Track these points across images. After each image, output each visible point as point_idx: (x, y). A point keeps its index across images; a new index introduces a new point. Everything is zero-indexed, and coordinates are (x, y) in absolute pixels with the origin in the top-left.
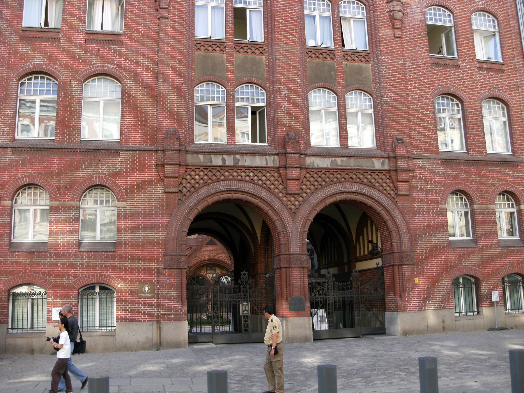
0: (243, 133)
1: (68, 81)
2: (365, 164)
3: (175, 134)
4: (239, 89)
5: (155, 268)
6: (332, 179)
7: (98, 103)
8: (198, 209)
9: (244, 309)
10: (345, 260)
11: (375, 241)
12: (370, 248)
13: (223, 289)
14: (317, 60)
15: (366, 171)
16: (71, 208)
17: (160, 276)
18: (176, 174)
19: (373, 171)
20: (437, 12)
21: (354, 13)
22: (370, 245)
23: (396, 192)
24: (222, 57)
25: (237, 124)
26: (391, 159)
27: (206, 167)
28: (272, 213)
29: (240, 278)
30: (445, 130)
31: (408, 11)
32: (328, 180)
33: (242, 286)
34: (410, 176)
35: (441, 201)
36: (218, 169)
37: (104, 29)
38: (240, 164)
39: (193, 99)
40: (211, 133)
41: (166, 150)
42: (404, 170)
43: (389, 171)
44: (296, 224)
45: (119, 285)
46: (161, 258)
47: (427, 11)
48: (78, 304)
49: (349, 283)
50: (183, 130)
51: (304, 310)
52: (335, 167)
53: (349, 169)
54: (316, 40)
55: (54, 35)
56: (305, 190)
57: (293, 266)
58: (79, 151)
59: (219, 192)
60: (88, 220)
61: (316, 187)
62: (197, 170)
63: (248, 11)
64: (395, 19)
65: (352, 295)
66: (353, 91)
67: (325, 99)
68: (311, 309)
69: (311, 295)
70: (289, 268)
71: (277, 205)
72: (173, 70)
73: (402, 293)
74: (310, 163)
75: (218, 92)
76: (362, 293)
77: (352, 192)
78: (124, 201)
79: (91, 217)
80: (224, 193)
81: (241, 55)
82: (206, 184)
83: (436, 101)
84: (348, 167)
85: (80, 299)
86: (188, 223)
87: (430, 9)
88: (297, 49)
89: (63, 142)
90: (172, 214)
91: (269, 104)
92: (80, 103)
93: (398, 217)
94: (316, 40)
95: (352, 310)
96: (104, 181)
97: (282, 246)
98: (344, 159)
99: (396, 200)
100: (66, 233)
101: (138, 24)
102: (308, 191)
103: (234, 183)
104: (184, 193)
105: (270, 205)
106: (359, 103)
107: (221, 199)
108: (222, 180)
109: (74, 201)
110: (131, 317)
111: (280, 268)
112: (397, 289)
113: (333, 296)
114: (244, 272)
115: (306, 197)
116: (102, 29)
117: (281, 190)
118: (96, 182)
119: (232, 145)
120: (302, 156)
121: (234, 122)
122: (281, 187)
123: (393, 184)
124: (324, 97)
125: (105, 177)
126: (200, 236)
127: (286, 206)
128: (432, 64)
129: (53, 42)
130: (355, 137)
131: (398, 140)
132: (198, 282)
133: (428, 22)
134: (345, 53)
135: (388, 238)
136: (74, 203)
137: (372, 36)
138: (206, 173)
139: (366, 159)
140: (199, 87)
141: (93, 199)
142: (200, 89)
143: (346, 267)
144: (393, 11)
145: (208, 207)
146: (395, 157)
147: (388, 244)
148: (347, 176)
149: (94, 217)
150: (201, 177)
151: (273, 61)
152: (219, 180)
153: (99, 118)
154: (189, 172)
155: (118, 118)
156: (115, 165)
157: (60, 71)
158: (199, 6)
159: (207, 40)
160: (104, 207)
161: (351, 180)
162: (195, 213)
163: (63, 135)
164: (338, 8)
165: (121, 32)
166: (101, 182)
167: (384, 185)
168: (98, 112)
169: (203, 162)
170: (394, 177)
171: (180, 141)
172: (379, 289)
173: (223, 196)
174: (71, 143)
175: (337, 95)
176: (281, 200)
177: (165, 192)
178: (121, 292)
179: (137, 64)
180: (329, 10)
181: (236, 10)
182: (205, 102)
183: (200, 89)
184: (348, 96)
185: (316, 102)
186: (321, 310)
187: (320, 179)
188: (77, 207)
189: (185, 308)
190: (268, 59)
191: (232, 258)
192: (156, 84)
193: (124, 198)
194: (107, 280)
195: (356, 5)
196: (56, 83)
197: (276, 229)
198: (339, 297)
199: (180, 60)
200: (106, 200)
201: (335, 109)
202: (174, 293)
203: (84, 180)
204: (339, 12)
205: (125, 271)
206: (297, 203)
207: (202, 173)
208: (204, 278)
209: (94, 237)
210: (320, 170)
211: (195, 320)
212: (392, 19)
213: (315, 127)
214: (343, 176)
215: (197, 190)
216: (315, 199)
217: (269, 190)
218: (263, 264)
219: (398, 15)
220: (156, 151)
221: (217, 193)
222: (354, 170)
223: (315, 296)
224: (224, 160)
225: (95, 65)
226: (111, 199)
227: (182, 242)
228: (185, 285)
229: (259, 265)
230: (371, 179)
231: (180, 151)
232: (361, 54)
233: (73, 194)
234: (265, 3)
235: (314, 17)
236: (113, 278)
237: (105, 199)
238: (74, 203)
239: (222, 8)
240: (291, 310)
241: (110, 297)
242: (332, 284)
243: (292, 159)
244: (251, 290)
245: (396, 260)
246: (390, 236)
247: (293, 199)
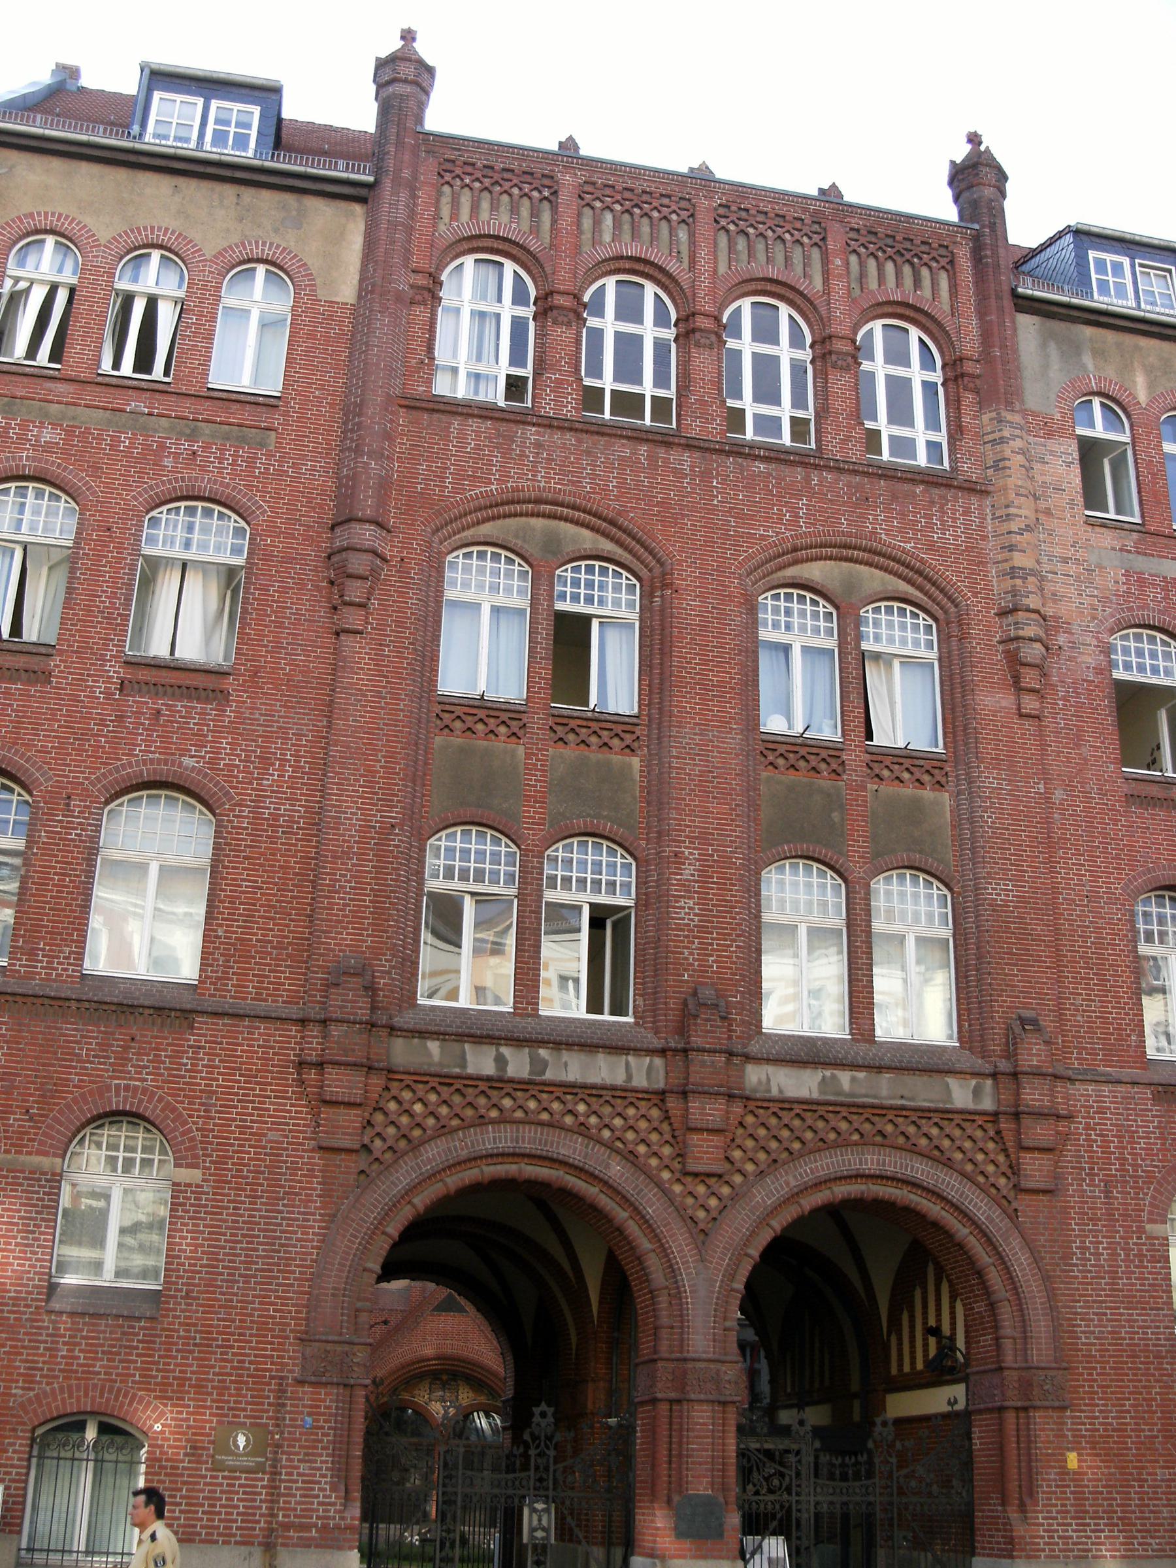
0: (564, 979)
1: (62, 798)
2: (923, 1092)
3: (361, 974)
4: (558, 851)
5: (272, 1377)
6: (821, 1135)
7: (143, 868)
8: (414, 1206)
9: (535, 1523)
10: (855, 1387)
11: (946, 1330)
12: (932, 1352)
13: (477, 1454)
14: (791, 777)
15: (925, 1113)
16: (35, 1175)
17: (284, 1405)
18: (357, 1095)
19: (947, 1114)
20: (1146, 646)
21: (904, 641)
22: (932, 1341)
23: (1014, 1179)
24: (513, 754)
25: (544, 952)
26: (1001, 1078)
27: (447, 1080)
28: (636, 1228)
29: (528, 1424)
30: (1164, 992)
31: (1062, 639)
32: (809, 1135)
33: (532, 1452)
34: (1058, 1133)
35: (1151, 1213)
36: (483, 1086)
37: (177, 655)
38: (549, 1075)
39: (420, 873)
40: (469, 977)
41: (331, 1020)
42: (1040, 1115)
43: (995, 1116)
44: (707, 1268)
45: (158, 1422)
46: (291, 1348)
47: (1116, 640)
48: (27, 1474)
49: (863, 1458)
50: (384, 963)
51: (721, 1535)
52: (831, 1098)
53: (873, 1107)
54: (789, 717)
55: (34, 663)
56: (738, 1165)
57: (693, 1396)
58: (74, 1005)
59: (481, 1157)
60: (83, 1212)
61: (774, 1156)
62: (421, 1086)
63: (595, 624)
64: (1023, 664)
65: (871, 1498)
66: (894, 873)
67: (810, 893)
68: (744, 1534)
69: (744, 1490)
70: (679, 1401)
71: (653, 1207)
72: (369, 784)
73: (1028, 1501)
74: (760, 1082)
75: (495, 855)
76: (901, 1492)
77: (882, 1177)
78: (195, 1166)
79: (94, 1203)
80: (495, 1160)
81: (570, 753)
82: (443, 1130)
83: (1140, 909)
84: (870, 1100)
85: (34, 1461)
86: (382, 1247)
87: (1125, 638)
88: (734, 739)
89: (29, 976)
90: (334, 1216)
91: (643, 901)
92: (91, 863)
93: (1020, 1261)
94: (789, 717)
95: (869, 1546)
96: (141, 1101)
97: (664, 1333)
98: (861, 1075)
99: (1015, 1205)
100: (14, 1251)
101: (277, 647)
102: (750, 1167)
103: (528, 1132)
104: (377, 1154)
105: (632, 1204)
106: (910, 909)
107: (486, 1179)
108: (493, 1122)
109: (46, 1154)
110: (185, 1526)
111: (654, 1401)
112: (1012, 1486)
113: (813, 1498)
114: (543, 1407)
115: (741, 1185)
116: (172, 652)
117: (666, 1161)
118: (118, 1103)
119: (529, 1015)
120: (736, 1060)
121: (537, 947)
122: (667, 1151)
123: (1007, 1156)
124: (809, 885)
125: (145, 1091)
126: (414, 1283)
127: (680, 1210)
128: (1131, 798)
129: (29, 682)
130: (897, 1005)
131: (1023, 1021)
132: (400, 1425)
133: (1119, 674)
134: (875, 758)
135: (986, 1321)
136: (45, 1162)
137: (953, 709)
138: (445, 1096)
139: (925, 1078)
140: (440, 839)
141: (104, 1152)
142: (443, 844)
143: (857, 1404)
144: (1017, 638)
145: (445, 1201)
146: (1015, 1075)
147: (987, 1340)
148: (867, 1126)
149: (102, 1204)
150: (431, 1108)
151: (661, 773)
152: (482, 1121)
153: (143, 907)
154: (394, 1092)
155: (199, 910)
156: (177, 1055)
157: (40, 768)
158: (454, 604)
159: (471, 702)
160: (135, 1180)
161: (879, 1139)
162: (405, 1215)
163: (32, 954)
164: (857, 626)
165: (227, 665)
166: (132, 1104)
167: (980, 1157)
168: (142, 893)
169: (440, 1064)
170: (1009, 1136)
171: (374, 996)
172: (955, 1483)
173: (492, 1168)
174: (55, 981)
175: (845, 880)
176: (666, 1192)
177: (321, 1148)
178: (162, 1446)
179: (266, 761)
180: (829, 632)
181: (562, 618)
182: (455, 885)
183: (443, 844)
184: (879, 885)
185: (782, 901)
186: (773, 1540)
187: (785, 1133)
188: (54, 1174)
189: (356, 1511)
190: (647, 765)
191: (509, 1358)
192: (317, 821)
193: (195, 1156)
194: (122, 1404)
195: (909, 620)
196: (27, 802)
197: (646, 1278)
198: (832, 1503)
199: (389, 756)
200: (143, 1160)
201: (840, 922)
202: (324, 1461)
203: (83, 1095)
204: (859, 637)
205: (182, 1380)
206: (713, 1202)
207: (433, 1097)
208: (422, 1415)
209: (98, 1266)
210: (786, 1106)
211: (382, 1546)
212: (1014, 662)
213: (775, 969)
214: (856, 1125)
215: (415, 1146)
216: (768, 1193)
217: (632, 1158)
218: (602, 1384)
219: (1033, 652)
220: (303, 1022)
221: (475, 1159)
222: (891, 1108)
223: (757, 1493)
224: (501, 1061)
225: (144, 755)
226: (156, 1158)
227: (359, 1305)
228: (358, 1438)
229: (590, 1385)
230: (938, 1137)
231: (373, 1025)
232: (921, 762)
233: (45, 1134)
234: (645, 602)
235: (786, 649)
236: (142, 1399)
237: (138, 1156)
238: (45, 1162)
239: (521, 612)
240: (680, 1534)
241: (128, 1458)
242: (812, 1459)
243: (705, 1068)
244: (560, 1466)
245: (1009, 1393)
246: (994, 1315)
247: (701, 1189)
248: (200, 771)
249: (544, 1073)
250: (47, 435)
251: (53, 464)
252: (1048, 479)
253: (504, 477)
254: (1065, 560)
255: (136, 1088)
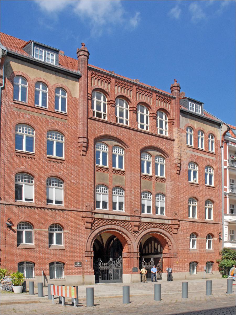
72: (88, 178)
78: (68, 230)
156: (64, 215)
179: (71, 174)
248: (61, 175)
249: (114, 218)
250: (27, 116)
251: (29, 122)
252: (182, 139)
253: (105, 132)
254: (183, 151)
255: (58, 220)
